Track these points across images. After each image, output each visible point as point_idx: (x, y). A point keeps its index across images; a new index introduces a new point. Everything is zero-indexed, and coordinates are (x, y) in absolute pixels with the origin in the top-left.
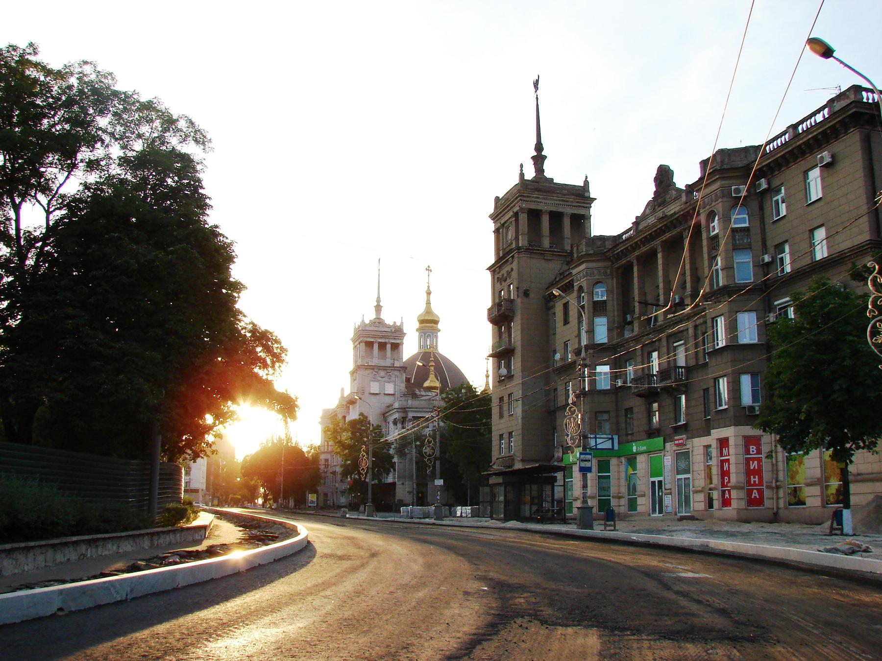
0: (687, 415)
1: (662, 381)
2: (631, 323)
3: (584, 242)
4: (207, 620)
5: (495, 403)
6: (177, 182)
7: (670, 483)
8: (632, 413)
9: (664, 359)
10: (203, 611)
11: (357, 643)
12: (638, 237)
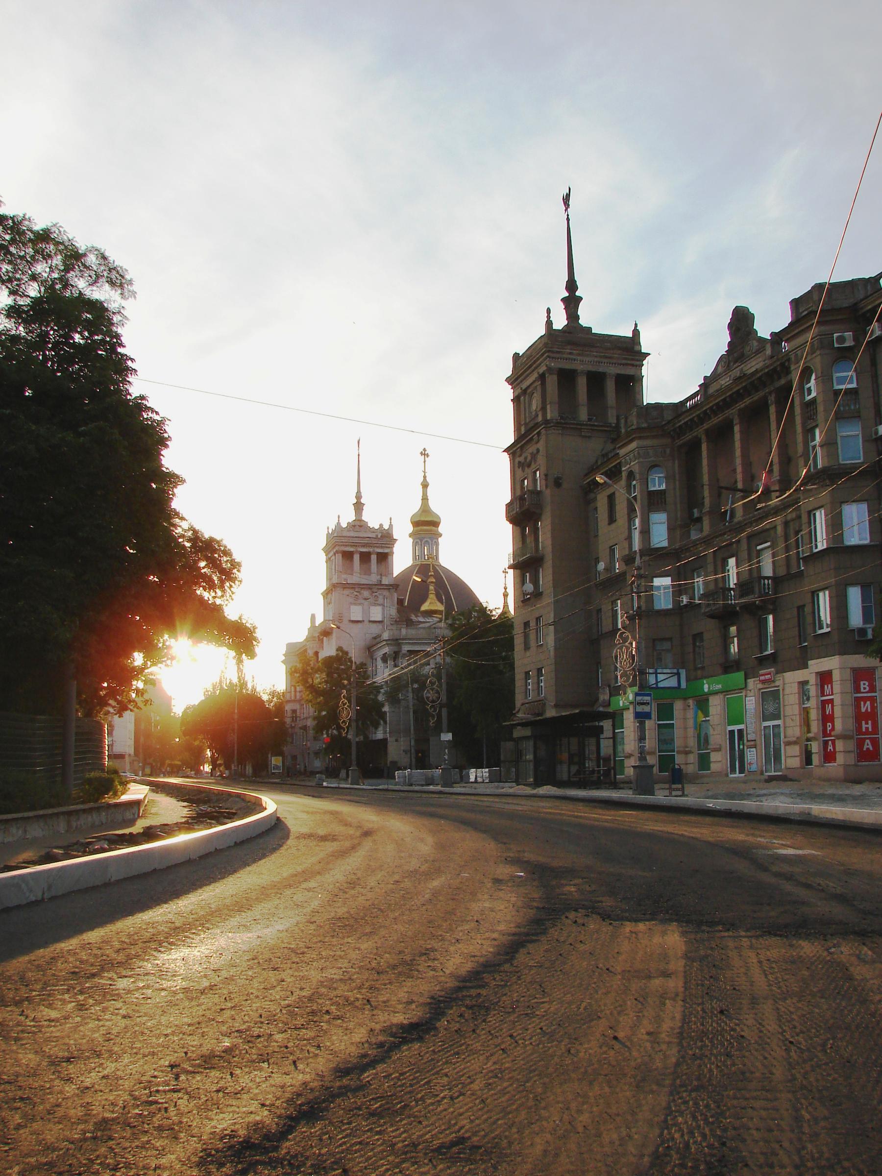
0: (776, 640)
1: (742, 596)
2: (699, 520)
3: (634, 411)
4: (153, 924)
5: (518, 631)
6: (88, 338)
7: (754, 733)
8: (702, 640)
9: (745, 567)
10: (146, 912)
11: (359, 949)
12: (708, 403)
